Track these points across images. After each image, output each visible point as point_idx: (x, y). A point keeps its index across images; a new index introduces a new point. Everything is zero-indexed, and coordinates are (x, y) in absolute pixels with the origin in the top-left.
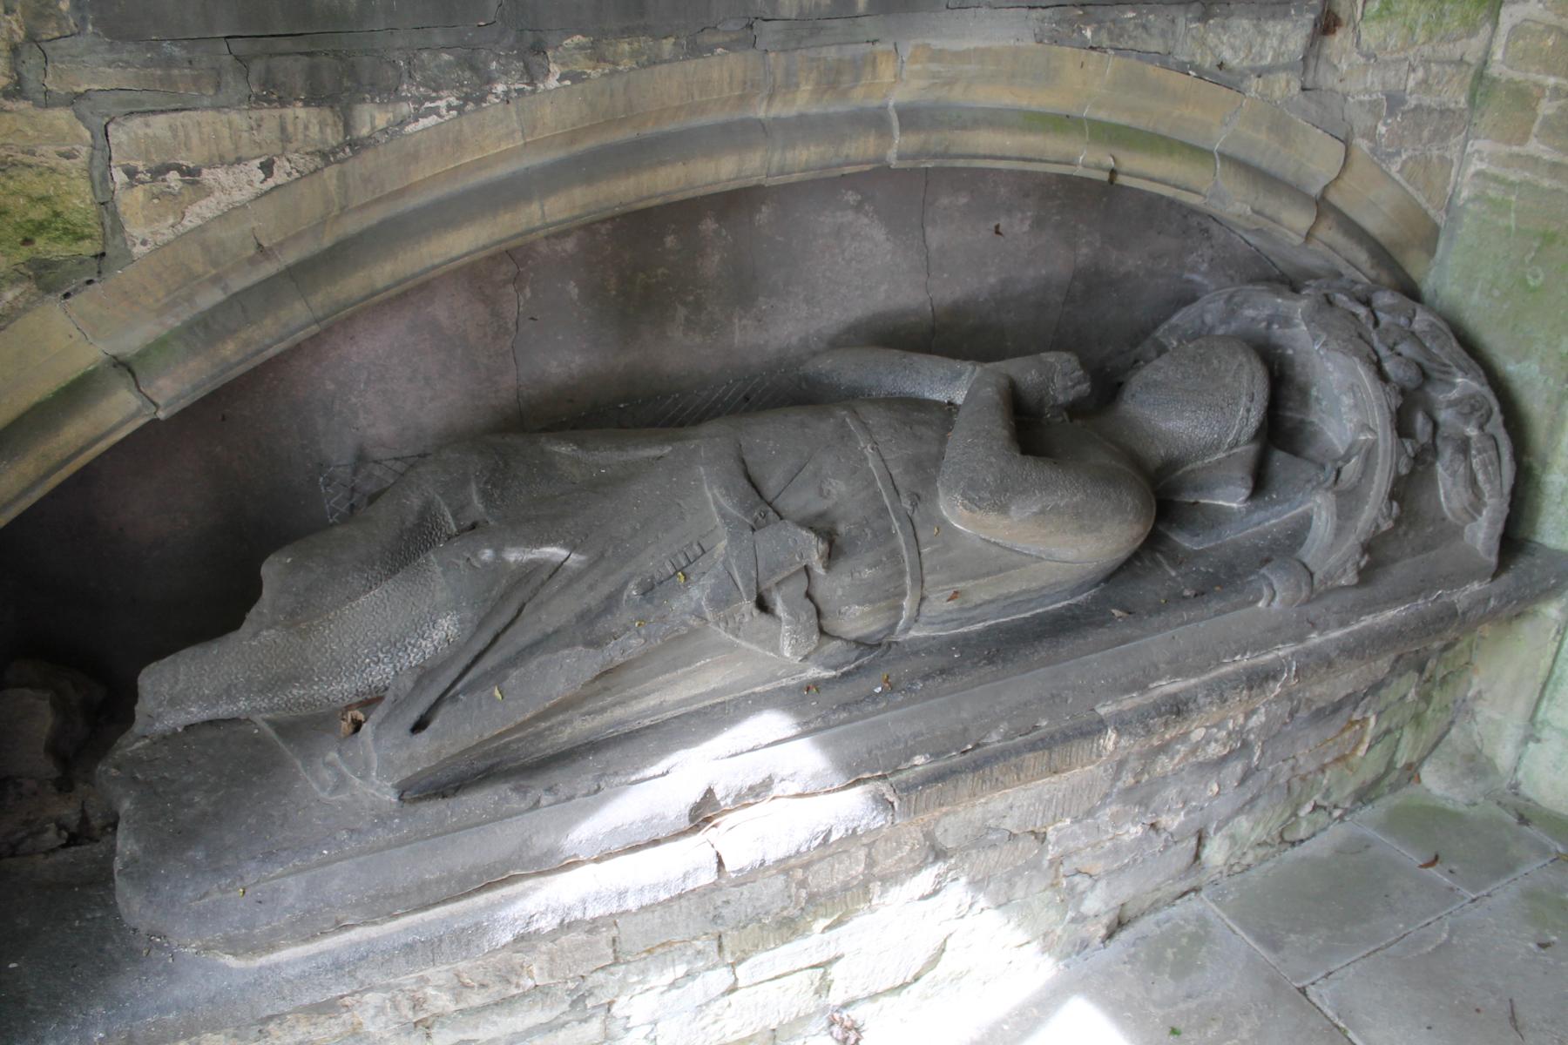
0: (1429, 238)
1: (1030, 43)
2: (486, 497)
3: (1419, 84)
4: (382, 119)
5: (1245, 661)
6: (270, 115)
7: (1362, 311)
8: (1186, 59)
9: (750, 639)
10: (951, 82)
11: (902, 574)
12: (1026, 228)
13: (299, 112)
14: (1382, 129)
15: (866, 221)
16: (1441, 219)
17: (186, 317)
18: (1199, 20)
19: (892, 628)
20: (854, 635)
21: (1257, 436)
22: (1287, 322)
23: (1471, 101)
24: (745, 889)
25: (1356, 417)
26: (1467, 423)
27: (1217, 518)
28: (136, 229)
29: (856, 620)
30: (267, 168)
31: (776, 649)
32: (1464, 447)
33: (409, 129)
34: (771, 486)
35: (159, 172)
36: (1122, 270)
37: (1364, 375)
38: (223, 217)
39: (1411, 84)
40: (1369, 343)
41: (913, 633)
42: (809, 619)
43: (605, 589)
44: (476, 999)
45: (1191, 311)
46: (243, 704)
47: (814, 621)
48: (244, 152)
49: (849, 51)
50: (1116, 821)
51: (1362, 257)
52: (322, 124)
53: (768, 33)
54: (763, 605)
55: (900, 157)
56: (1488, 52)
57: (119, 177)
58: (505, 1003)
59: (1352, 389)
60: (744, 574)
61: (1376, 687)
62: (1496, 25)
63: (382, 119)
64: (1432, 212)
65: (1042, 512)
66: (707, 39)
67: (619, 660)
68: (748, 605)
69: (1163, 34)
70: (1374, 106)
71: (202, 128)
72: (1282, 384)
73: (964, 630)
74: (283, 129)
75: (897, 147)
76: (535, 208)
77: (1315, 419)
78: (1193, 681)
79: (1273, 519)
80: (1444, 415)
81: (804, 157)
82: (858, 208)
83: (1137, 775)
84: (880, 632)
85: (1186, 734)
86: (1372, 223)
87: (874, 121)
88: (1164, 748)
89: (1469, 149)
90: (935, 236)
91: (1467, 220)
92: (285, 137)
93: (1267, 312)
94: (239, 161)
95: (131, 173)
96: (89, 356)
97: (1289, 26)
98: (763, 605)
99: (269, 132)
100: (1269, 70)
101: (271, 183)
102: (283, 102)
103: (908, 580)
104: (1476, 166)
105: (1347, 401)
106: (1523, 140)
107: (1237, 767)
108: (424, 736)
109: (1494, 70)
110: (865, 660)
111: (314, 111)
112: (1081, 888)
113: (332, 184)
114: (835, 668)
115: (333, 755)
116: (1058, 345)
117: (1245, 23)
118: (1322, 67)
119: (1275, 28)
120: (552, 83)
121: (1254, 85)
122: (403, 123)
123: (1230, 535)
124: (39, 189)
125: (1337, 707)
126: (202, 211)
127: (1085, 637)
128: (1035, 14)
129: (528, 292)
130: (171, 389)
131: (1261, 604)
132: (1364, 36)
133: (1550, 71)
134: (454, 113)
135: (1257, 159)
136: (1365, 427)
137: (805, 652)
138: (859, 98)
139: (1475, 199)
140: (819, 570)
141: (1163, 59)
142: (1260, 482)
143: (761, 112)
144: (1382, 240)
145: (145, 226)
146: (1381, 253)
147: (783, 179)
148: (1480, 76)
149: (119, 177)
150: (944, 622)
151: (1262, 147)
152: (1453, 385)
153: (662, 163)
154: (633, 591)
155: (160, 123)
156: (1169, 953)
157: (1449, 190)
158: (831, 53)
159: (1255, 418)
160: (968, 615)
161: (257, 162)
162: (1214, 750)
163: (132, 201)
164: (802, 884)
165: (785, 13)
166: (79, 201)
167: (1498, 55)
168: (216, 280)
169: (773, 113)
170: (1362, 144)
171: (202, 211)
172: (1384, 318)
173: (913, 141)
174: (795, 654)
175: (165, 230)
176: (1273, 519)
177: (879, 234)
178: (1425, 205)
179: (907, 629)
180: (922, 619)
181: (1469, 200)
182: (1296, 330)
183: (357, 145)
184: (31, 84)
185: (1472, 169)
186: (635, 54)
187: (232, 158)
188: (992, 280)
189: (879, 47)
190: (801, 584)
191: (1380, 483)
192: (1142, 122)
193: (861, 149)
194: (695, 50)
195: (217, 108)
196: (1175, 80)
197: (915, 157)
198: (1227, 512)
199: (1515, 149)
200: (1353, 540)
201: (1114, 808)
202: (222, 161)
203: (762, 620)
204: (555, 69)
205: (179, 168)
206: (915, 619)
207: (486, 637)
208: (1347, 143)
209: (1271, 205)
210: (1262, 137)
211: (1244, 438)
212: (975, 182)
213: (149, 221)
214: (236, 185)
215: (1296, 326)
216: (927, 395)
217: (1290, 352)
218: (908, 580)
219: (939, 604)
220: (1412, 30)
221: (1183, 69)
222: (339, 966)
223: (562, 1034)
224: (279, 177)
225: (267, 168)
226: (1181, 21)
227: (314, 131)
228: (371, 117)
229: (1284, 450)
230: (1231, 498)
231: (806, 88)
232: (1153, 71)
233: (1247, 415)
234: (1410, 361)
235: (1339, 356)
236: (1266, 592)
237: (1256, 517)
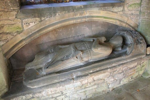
2: (53, 50)
3: (134, 12)
4: (44, 19)
6: (35, 19)
7: (131, 32)
9: (76, 60)
10: (91, 14)
13: (37, 18)
17: (29, 35)
20: (85, 61)
22: (124, 34)
23: (140, 14)
24: (76, 83)
27: (118, 51)
28: (25, 28)
30: (35, 23)
31: (78, 61)
34: (77, 48)
35: (27, 23)
36: (110, 31)
38: (31, 27)
39: (134, 12)
40: (132, 35)
41: (91, 61)
43: (63, 56)
44: (53, 93)
45: (116, 34)
46: (34, 67)
49: (82, 12)
50: (111, 78)
52: (39, 19)
53: (75, 10)
55: (87, 20)
57: (23, 24)
58: (56, 93)
59: (130, 39)
62: (141, 7)
63: (44, 19)
66: (70, 11)
70: (130, 14)
71: (29, 20)
72: (124, 40)
75: (87, 19)
76: (56, 25)
77: (128, 42)
79: (124, 51)
81: (79, 21)
82: (85, 26)
83: (113, 74)
85: (117, 70)
86: (132, 25)
87: (85, 17)
88: (115, 71)
91: (140, 24)
93: (122, 33)
94: (33, 22)
95: (24, 24)
96: (21, 39)
98: (77, 58)
99: (35, 20)
100: (120, 11)
101: (35, 24)
102: (36, 18)
105: (130, 40)
106: (145, 16)
112: (108, 85)
113: (40, 24)
115: (41, 71)
116: (103, 36)
121: (118, 13)
122: (45, 19)
123: (120, 52)
124: (18, 25)
125: (132, 68)
126: (30, 26)
127: (97, 49)
130: (28, 41)
133: (146, 10)
135: (120, 19)
138: (83, 15)
141: (110, 11)
143: (75, 17)
145: (25, 28)
147: (77, 23)
148: (140, 11)
149: (23, 24)
151: (120, 18)
153: (67, 21)
154: (65, 57)
155: (26, 20)
156: (118, 91)
158: (80, 12)
159: (122, 42)
162: (120, 72)
163: (24, 26)
164: (82, 83)
166: (21, 26)
168: (31, 32)
169: (76, 17)
171: (30, 26)
172: (133, 33)
175: (27, 28)
176: (124, 51)
179: (90, 60)
184: (17, 17)
185: (140, 20)
186: (64, 13)
187: (32, 22)
188: (98, 32)
192: (109, 17)
193: (84, 20)
194: (69, 12)
195: (31, 18)
197: (89, 20)
199: (144, 17)
201: (111, 77)
202: (31, 22)
204: (57, 14)
205: (28, 23)
208: (128, 18)
209: (122, 23)
211: (121, 44)
212: (95, 22)
213: (26, 27)
214: (32, 24)
220: (133, 8)
222: (40, 88)
223: (61, 96)
224: (36, 24)
225: (35, 23)
228: (43, 19)
230: (120, 49)
231: (78, 15)
232: (109, 12)
237: (122, 51)
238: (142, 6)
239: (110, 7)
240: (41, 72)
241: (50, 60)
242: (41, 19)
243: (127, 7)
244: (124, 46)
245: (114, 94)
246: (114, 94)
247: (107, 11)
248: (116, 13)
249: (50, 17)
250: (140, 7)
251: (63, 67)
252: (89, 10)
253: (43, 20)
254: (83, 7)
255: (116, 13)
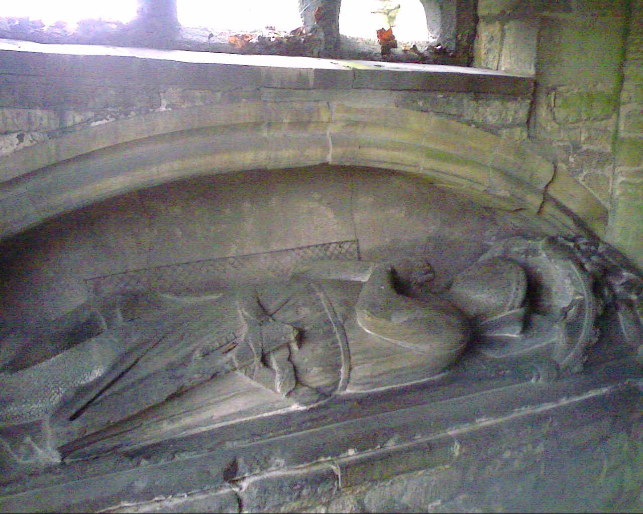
0: (604, 217)
1: (392, 107)
4: (78, 119)
5: (526, 411)
8: (469, 118)
11: (339, 354)
12: (403, 215)
14: (572, 159)
15: (324, 208)
16: (608, 206)
18: (474, 100)
19: (336, 384)
20: (314, 385)
21: (523, 304)
23: (614, 149)
25: (573, 288)
26: (631, 292)
29: (315, 377)
32: (630, 304)
33: (93, 124)
37: (575, 269)
41: (348, 391)
42: (290, 372)
43: (183, 352)
47: (293, 373)
48: (10, 129)
51: (570, 222)
52: (49, 118)
54: (265, 361)
56: (617, 126)
60: (256, 345)
61: (603, 439)
62: (618, 116)
64: (603, 202)
65: (409, 320)
67: (189, 384)
68: (257, 360)
69: (456, 106)
70: (566, 149)
73: (375, 390)
74: (29, 119)
78: (500, 420)
80: (618, 290)
82: (319, 201)
84: (326, 386)
85: (500, 453)
86: (572, 206)
89: (616, 172)
90: (358, 218)
91: (620, 205)
92: (29, 122)
97: (518, 105)
98: (265, 361)
103: (342, 357)
104: (621, 179)
107: (532, 477)
108: (76, 422)
109: (622, 134)
110: (322, 402)
111: (46, 112)
114: (306, 404)
117: (497, 103)
118: (538, 129)
119: (512, 106)
120: (163, 109)
121: (505, 132)
122: (89, 121)
128: (395, 93)
129: (155, 231)
131: (533, 381)
132: (556, 114)
134: (114, 119)
136: (577, 293)
137: (289, 390)
139: (623, 195)
140: (295, 347)
141: (459, 117)
142: (526, 324)
144: (581, 216)
146: (580, 223)
150: (363, 384)
152: (622, 277)
154: (198, 355)
157: (610, 191)
160: (377, 380)
161: (16, 135)
165: (275, 85)
167: (622, 127)
170: (562, 166)
173: (340, 151)
174: (283, 390)
176: (535, 344)
177: (330, 214)
178: (599, 199)
179: (344, 388)
180: (352, 381)
181: (620, 196)
182: (540, 257)
183: (64, 130)
186: (204, 98)
189: (320, 105)
190: (285, 352)
191: (587, 321)
196: (465, 128)
198: (512, 339)
200: (578, 348)
201: (415, 331)
203: (265, 371)
204: (164, 102)
206: (348, 381)
207: (115, 374)
209: (519, 192)
210: (511, 158)
211: (517, 304)
215: (541, 254)
216: (352, 279)
217: (539, 270)
218: (342, 357)
219: (360, 372)
221: (469, 123)
224: (27, 143)
225: (21, 138)
226: (465, 101)
227: (45, 122)
229: (539, 314)
230: (513, 333)
232: (454, 124)
233: (518, 293)
234: (598, 265)
235: (562, 262)
236: (535, 374)
238: (624, 111)
239: (461, 95)
240: (32, 451)
241: (98, 373)
242: (62, 117)
243: (549, 106)
244: (537, 319)
245: (229, 46)
246: (229, 46)
247: (444, 119)
248: (493, 130)
249: (121, 112)
250: (614, 116)
251: (482, 422)
252: (347, 104)
253: (74, 126)
254: (315, 83)
255: (493, 130)
